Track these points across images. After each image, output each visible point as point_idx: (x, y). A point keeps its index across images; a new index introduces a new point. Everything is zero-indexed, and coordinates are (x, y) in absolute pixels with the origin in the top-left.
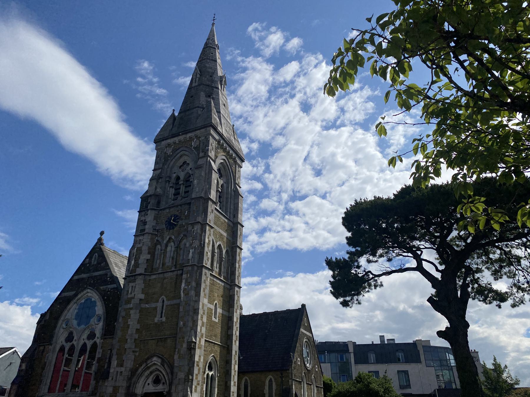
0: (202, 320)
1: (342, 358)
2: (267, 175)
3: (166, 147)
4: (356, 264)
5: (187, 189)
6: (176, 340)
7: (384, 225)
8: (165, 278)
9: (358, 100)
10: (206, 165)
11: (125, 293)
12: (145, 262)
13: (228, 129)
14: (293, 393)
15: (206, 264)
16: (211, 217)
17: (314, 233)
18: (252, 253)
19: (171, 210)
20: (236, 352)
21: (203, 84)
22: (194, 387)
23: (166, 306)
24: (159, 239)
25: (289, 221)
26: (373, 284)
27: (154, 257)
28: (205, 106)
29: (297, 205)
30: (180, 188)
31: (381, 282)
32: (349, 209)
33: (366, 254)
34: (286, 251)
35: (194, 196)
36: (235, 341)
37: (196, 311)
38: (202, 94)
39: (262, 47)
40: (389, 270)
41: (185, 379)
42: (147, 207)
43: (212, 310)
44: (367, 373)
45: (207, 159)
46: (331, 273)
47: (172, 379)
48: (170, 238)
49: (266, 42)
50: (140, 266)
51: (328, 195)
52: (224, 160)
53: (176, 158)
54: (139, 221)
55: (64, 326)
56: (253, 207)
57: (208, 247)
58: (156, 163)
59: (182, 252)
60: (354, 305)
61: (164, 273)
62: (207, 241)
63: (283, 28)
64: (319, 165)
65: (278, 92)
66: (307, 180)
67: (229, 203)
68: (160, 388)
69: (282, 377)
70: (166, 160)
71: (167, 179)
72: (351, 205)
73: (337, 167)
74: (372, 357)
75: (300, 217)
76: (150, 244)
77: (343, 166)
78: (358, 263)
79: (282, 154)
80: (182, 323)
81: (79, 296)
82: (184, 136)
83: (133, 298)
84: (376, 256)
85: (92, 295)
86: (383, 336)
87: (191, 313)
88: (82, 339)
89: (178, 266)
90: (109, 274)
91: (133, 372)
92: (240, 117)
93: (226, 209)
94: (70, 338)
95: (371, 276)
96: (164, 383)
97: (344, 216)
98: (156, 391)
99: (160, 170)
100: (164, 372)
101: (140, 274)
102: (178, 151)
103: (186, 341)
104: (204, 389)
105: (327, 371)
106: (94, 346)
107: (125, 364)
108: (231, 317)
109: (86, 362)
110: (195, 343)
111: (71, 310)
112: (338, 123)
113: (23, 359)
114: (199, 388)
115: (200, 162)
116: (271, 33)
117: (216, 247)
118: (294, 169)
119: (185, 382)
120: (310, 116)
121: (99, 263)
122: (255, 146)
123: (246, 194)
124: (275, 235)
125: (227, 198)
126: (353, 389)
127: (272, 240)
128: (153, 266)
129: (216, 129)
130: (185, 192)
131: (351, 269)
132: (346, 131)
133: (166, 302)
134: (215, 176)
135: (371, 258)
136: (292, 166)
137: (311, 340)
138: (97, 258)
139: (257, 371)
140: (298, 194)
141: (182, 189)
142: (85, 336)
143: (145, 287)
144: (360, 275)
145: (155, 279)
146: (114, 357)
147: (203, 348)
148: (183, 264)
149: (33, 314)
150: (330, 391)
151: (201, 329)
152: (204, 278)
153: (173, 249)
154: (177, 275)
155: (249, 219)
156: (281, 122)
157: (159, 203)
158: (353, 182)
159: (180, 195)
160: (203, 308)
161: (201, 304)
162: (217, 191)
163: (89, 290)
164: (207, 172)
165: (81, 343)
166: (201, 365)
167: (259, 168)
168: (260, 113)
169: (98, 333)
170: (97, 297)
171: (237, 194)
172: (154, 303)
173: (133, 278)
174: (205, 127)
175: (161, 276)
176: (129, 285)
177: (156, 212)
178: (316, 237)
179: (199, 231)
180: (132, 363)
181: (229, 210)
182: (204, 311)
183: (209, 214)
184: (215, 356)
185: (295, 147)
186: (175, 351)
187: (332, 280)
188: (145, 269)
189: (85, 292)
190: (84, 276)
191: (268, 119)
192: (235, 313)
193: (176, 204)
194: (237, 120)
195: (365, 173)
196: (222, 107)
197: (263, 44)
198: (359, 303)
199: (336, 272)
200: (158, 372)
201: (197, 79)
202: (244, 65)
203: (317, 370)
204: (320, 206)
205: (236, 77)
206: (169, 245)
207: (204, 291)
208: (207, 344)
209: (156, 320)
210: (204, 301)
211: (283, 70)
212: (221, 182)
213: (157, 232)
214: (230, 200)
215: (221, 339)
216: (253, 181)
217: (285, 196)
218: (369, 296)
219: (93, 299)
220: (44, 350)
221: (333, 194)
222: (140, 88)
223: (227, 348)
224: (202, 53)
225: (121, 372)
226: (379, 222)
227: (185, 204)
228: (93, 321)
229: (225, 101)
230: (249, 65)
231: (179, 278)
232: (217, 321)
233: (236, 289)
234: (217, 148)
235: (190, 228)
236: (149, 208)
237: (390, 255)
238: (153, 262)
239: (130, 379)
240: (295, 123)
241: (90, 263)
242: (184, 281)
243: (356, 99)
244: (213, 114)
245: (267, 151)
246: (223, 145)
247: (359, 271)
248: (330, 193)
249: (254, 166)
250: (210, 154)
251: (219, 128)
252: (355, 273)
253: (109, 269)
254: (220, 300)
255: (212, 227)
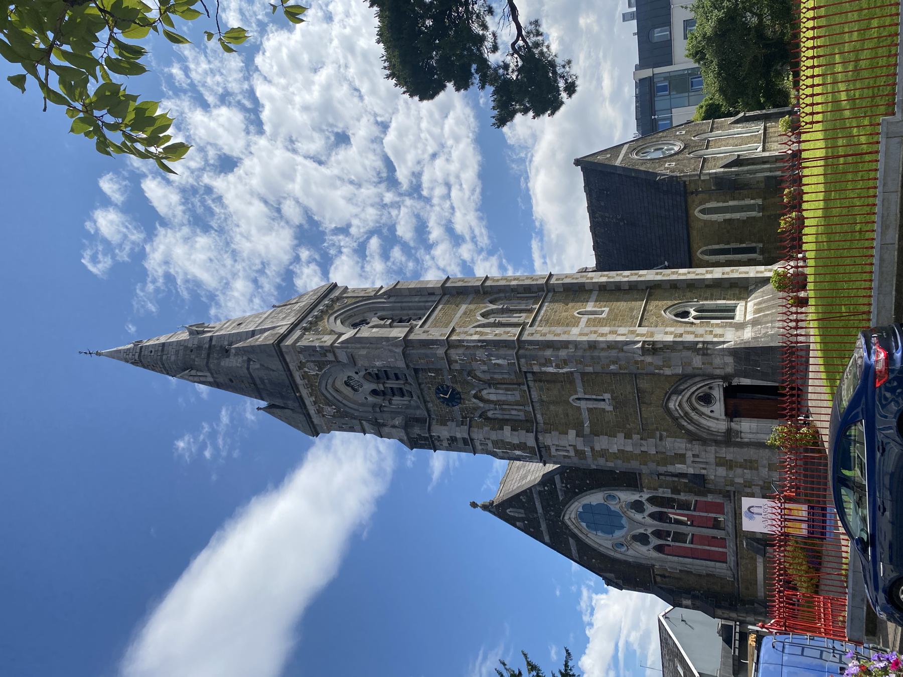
0: (607, 334)
1: (664, 89)
2: (353, 230)
3: (323, 416)
4: (501, 71)
5: (392, 376)
6: (640, 374)
7: (429, 23)
8: (541, 401)
9: (204, 66)
10: (347, 348)
11: (567, 460)
12: (516, 433)
13: (282, 316)
14: (723, 172)
15: (515, 335)
16: (437, 333)
17: (450, 142)
18: (491, 253)
19: (428, 399)
20: (657, 274)
21: (207, 363)
22: (715, 340)
23: (585, 394)
24: (477, 414)
25: (432, 189)
26: (534, 39)
27: (507, 420)
28: (245, 358)
29: (402, 174)
30: (392, 388)
31: (531, 23)
32: (404, 89)
33: (482, 54)
34: (483, 193)
35: (401, 364)
36: (640, 276)
37: (593, 346)
38: (225, 363)
39: (127, 248)
40: (507, 9)
41: (704, 354)
42: (426, 439)
43: (589, 320)
44: (688, 41)
45: (337, 347)
46: (519, 117)
47: (704, 375)
48: (476, 396)
49: (115, 239)
50: (523, 441)
51: (379, 119)
52: (336, 318)
53: (340, 399)
54: (450, 448)
55: (624, 549)
56: (413, 251)
57: (487, 334)
58: (352, 429)
59: (496, 376)
60: (573, 72)
61: (532, 402)
62: (476, 337)
63: (87, 213)
64: (328, 138)
65: (202, 212)
66: (356, 158)
67: (410, 304)
68: (718, 394)
69: (697, 193)
70: (345, 415)
71: (378, 409)
72: (396, 85)
73: (327, 107)
74: (658, 34)
75: (422, 168)
76: (486, 429)
77: (327, 88)
78: (499, 67)
79: (311, 204)
80: (612, 367)
81: (576, 531)
82: (301, 388)
83: (575, 446)
84: (483, 35)
85: (572, 513)
86: (624, 15)
87: (596, 354)
88: (643, 520)
89: (520, 381)
90: (538, 489)
91: (693, 437)
92: (255, 281)
93: (420, 309)
94: (643, 539)
95: (521, 43)
96: (711, 388)
97: (417, 98)
98: (722, 398)
99: (364, 422)
100: (693, 389)
101: (537, 439)
102: (328, 395)
103: (642, 358)
104: (719, 321)
105: (686, 113)
106: (652, 500)
107: (681, 452)
108: (600, 286)
109: (678, 511)
110: (644, 342)
111: (598, 541)
112: (248, 104)
113: (676, 604)
114: (718, 331)
115: (343, 357)
116: (97, 230)
117: (484, 321)
118: (338, 183)
119: (707, 355)
120: (241, 156)
121: (521, 505)
122: (305, 254)
123: (389, 264)
124: (458, 214)
125: (402, 309)
126: (714, 66)
127: (466, 220)
128: (521, 421)
129: (284, 337)
130: (397, 378)
131: (510, 80)
132: (261, 89)
133: (580, 395)
134: (365, 332)
135: (488, 44)
136: (334, 187)
137: (636, 146)
138: (515, 510)
139: (686, 207)
140: (384, 175)
141: (392, 384)
142: (638, 517)
143: (557, 430)
144: (520, 63)
145: (542, 415)
146: (671, 469)
147: (653, 329)
148: (515, 372)
149: (607, 592)
150: (719, 107)
151: (621, 334)
152: (537, 337)
153: (493, 390)
154: (535, 381)
155: (433, 258)
156: (257, 209)
157: (420, 421)
158: (352, 71)
159: (402, 386)
160: (587, 335)
161: (579, 339)
162: (391, 326)
163: (566, 518)
164: (358, 346)
165: (649, 521)
166: (680, 330)
167: (342, 244)
168: (245, 247)
169: (635, 497)
170: (576, 503)
171: (393, 293)
172: (581, 414)
173: (543, 450)
174: (281, 354)
175: (537, 406)
176: (554, 456)
177: (434, 422)
178: (457, 139)
179: (460, 351)
180: (678, 440)
181: (422, 304)
182: (591, 332)
183: (430, 337)
184: (665, 307)
185: (299, 179)
186: (659, 374)
187: (531, 114)
188: (527, 432)
189: (569, 523)
190: (543, 527)
191: (254, 231)
192: (594, 281)
193: (419, 392)
194: (262, 287)
195: (334, 49)
196: (242, 329)
197: (120, 246)
198: (569, 62)
199: (518, 107)
200: (693, 399)
201: (199, 374)
202: (161, 280)
203: (684, 132)
204: (401, 135)
205: (186, 295)
206: (486, 397)
207: (559, 335)
208: (645, 323)
209: (610, 408)
210: (575, 334)
211: (162, 208)
212: (375, 321)
213: (466, 420)
214: (405, 303)
215: (636, 300)
216: (367, 253)
217: (389, 197)
218: (554, 43)
219: (581, 510)
220: (661, 576)
221: (378, 110)
222: (224, 454)
223: (651, 290)
224: (153, 370)
225: (694, 456)
226: (423, 32)
227: (417, 378)
228: (614, 506)
229: (233, 323)
230: (160, 271)
231: (539, 377)
232: (607, 309)
233: (553, 281)
234: (317, 332)
235: (456, 366)
236: (427, 435)
237: (482, 10)
238: (516, 420)
239: (704, 442)
240: (255, 182)
241: (522, 520)
242: (544, 369)
243: (200, 70)
244: (258, 343)
245: (311, 234)
246: (311, 323)
247: (512, 66)
248: (375, 115)
249: (340, 252)
250: (329, 343)
251: (282, 331)
252: (516, 73)
253: (530, 489)
254: (573, 307)
255: (453, 330)
